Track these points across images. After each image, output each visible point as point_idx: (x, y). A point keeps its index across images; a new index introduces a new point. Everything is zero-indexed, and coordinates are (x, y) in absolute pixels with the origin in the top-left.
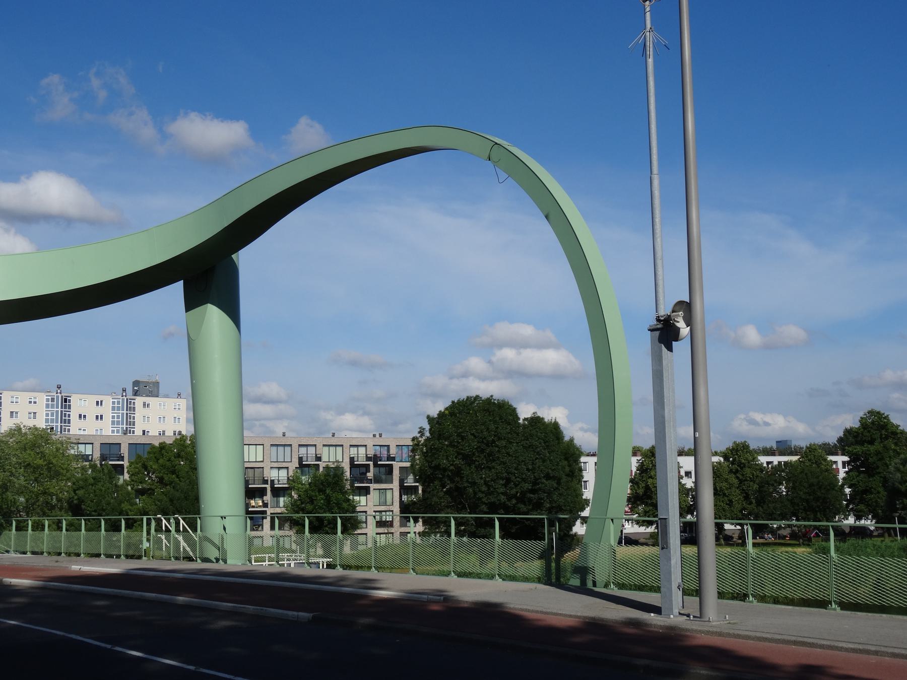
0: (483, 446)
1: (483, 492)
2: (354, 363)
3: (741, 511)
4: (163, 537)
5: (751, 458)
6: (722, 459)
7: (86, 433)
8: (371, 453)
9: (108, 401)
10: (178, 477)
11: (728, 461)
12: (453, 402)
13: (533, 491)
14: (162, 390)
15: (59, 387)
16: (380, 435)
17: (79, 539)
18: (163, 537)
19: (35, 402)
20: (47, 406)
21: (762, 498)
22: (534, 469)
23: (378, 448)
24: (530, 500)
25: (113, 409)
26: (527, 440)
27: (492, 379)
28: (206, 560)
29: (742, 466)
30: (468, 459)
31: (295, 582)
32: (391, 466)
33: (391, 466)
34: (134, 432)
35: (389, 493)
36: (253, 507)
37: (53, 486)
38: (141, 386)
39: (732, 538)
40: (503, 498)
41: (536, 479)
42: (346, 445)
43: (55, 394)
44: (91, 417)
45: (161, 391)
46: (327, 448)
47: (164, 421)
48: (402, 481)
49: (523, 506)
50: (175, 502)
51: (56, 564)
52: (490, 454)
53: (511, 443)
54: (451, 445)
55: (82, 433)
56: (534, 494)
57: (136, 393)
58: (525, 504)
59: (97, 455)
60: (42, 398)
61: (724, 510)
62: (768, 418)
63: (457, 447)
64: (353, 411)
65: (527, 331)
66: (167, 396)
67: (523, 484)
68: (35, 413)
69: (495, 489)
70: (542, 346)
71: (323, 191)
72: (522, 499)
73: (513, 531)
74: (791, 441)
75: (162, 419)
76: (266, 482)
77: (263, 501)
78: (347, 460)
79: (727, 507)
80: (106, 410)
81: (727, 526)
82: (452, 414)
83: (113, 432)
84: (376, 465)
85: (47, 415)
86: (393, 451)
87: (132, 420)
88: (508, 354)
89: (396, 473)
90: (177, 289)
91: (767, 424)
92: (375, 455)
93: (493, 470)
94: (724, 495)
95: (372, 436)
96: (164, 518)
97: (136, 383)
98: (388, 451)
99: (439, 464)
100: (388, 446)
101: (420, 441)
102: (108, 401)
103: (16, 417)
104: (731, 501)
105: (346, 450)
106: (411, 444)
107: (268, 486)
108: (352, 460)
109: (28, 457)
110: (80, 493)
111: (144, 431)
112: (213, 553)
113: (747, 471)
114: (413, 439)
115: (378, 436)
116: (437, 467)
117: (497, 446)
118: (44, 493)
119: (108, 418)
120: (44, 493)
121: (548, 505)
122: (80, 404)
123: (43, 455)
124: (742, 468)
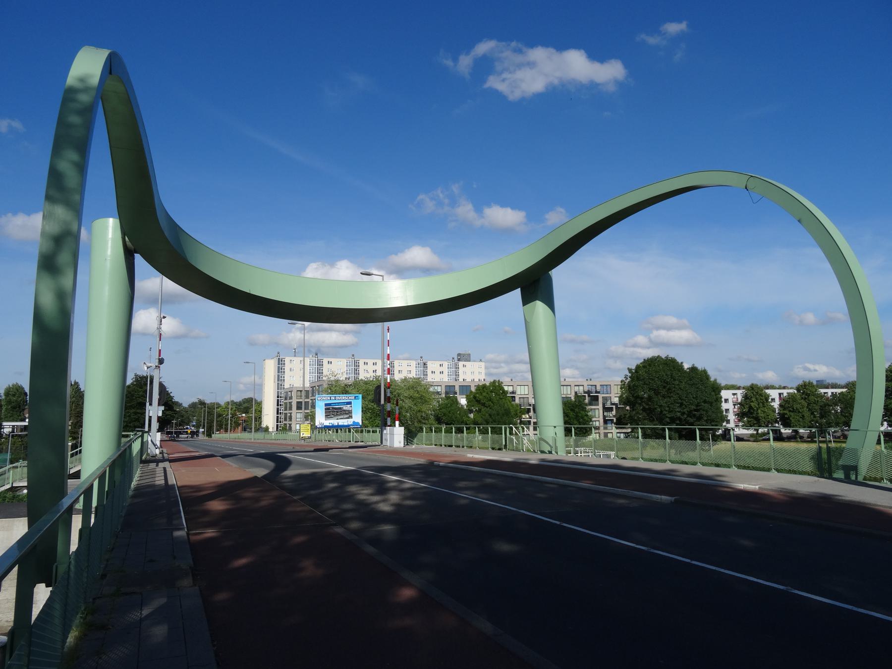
0: (665, 385)
1: (666, 411)
2: (572, 341)
3: (810, 422)
4: (514, 438)
5: (814, 390)
6: (796, 392)
7: (435, 380)
8: (586, 390)
9: (446, 364)
10: (492, 402)
11: (800, 392)
12: (645, 360)
13: (695, 410)
14: (472, 358)
15: (421, 357)
16: (591, 380)
17: (441, 436)
18: (514, 438)
19: (410, 366)
20: (416, 367)
21: (824, 413)
22: (697, 397)
23: (590, 386)
24: (694, 415)
25: (347, 366)
26: (691, 380)
27: (649, 348)
28: (542, 452)
29: (808, 395)
30: (657, 393)
31: (615, 469)
32: (598, 396)
33: (598, 396)
34: (459, 380)
35: (597, 411)
36: (524, 418)
37: (424, 408)
38: (462, 356)
39: (803, 437)
40: (679, 414)
41: (698, 403)
42: (573, 385)
43: (419, 361)
44: (437, 372)
45: (471, 360)
46: (578, 387)
47: (474, 374)
48: (604, 405)
49: (690, 419)
50: (492, 416)
51: (454, 453)
52: (669, 389)
53: (682, 382)
54: (645, 384)
55: (433, 380)
56: (697, 412)
57: (459, 360)
58: (692, 418)
59: (443, 391)
60: (413, 363)
61: (799, 421)
62: (817, 367)
63: (649, 385)
64: (572, 367)
65: (672, 320)
66: (474, 361)
67: (690, 406)
68: (410, 371)
69: (673, 409)
70: (679, 328)
71: (615, 224)
72: (690, 414)
73: (684, 433)
74: (826, 380)
75: (473, 373)
76: (530, 405)
77: (529, 416)
78: (573, 394)
79: (801, 420)
80: (445, 369)
81: (801, 431)
82: (644, 367)
83: (448, 380)
84: (589, 396)
85: (416, 372)
86: (598, 388)
87: (321, 371)
88: (663, 333)
89: (600, 400)
90: (517, 293)
91: (815, 370)
92: (589, 391)
93: (672, 398)
94: (799, 412)
95: (510, 380)
96: (526, 427)
97: (459, 355)
98: (596, 388)
99: (639, 395)
100: (596, 385)
101: (625, 383)
102: (446, 364)
103: (402, 373)
104: (803, 416)
105: (573, 388)
106: (620, 384)
107: (531, 408)
108: (576, 393)
109: (411, 393)
110: (443, 410)
111: (464, 379)
112: (546, 448)
113: (812, 398)
114: (622, 381)
115: (589, 380)
116: (637, 397)
117: (674, 384)
118: (419, 411)
119: (446, 373)
120: (419, 411)
121: (706, 418)
122: (432, 366)
123: (418, 392)
124: (809, 396)
